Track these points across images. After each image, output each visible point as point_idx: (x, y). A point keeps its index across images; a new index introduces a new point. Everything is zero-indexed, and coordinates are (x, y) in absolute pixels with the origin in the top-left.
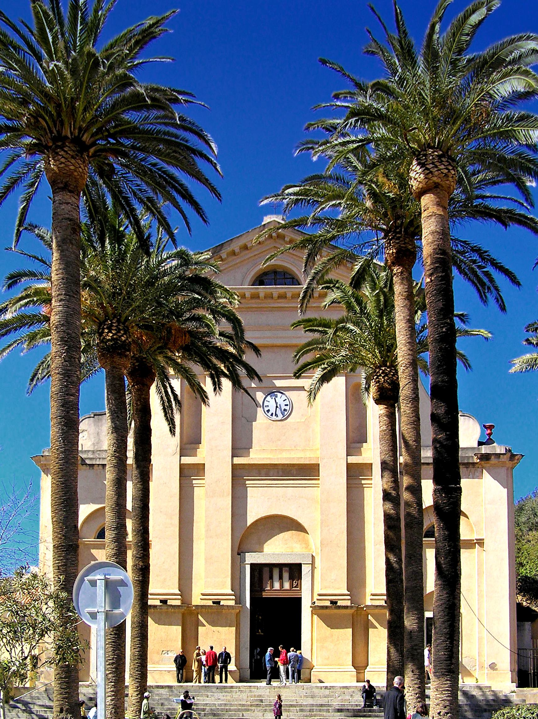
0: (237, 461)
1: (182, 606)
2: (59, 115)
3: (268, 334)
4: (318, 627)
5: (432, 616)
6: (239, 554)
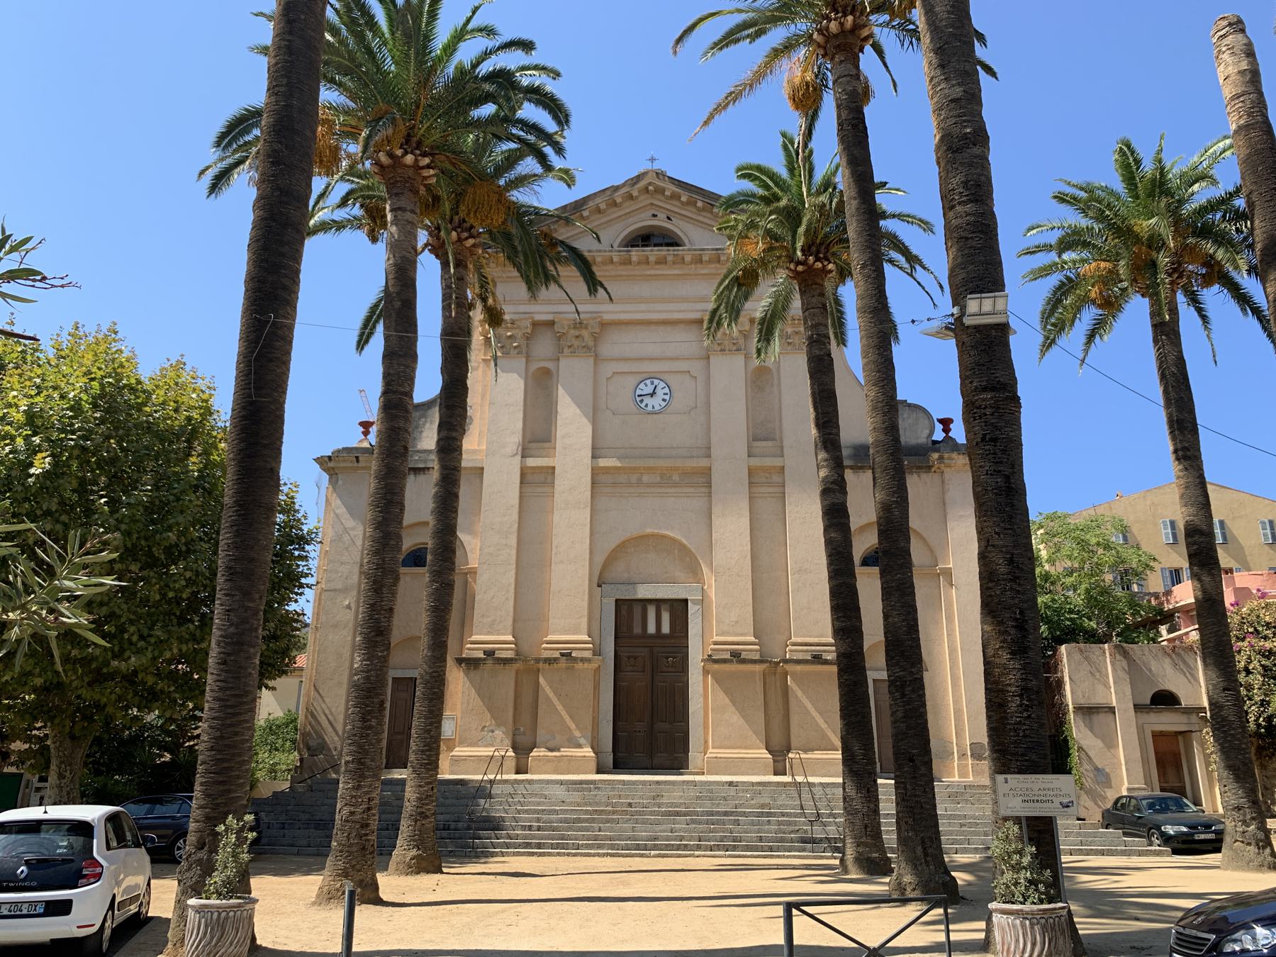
2: (360, 37)
5: (261, 885)
6: (599, 586)
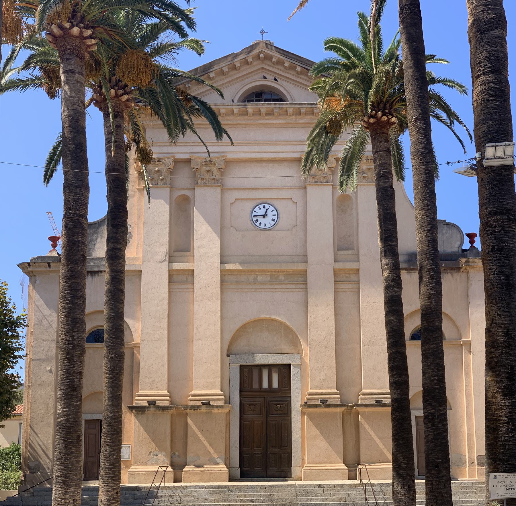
0: (176, 266)
1: (171, 407)
3: (256, 148)
4: (308, 426)
6: (228, 355)
